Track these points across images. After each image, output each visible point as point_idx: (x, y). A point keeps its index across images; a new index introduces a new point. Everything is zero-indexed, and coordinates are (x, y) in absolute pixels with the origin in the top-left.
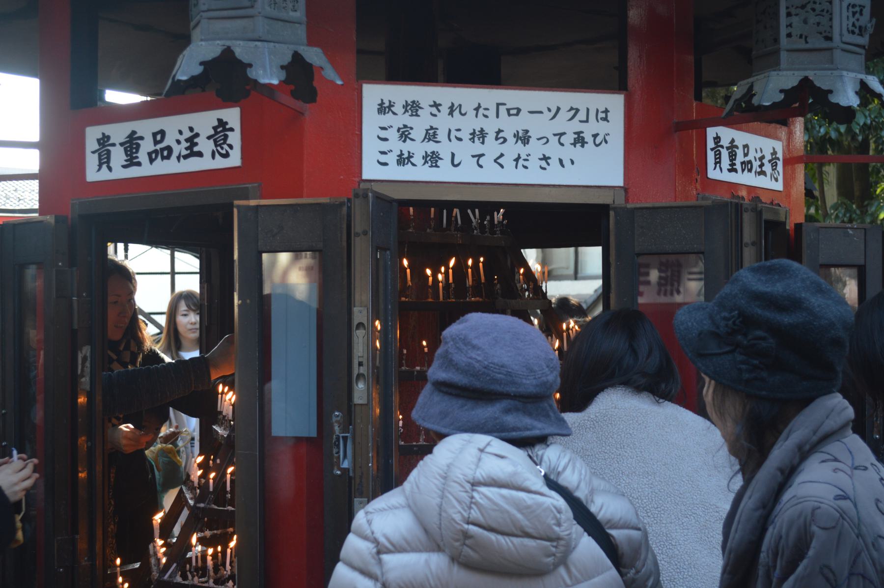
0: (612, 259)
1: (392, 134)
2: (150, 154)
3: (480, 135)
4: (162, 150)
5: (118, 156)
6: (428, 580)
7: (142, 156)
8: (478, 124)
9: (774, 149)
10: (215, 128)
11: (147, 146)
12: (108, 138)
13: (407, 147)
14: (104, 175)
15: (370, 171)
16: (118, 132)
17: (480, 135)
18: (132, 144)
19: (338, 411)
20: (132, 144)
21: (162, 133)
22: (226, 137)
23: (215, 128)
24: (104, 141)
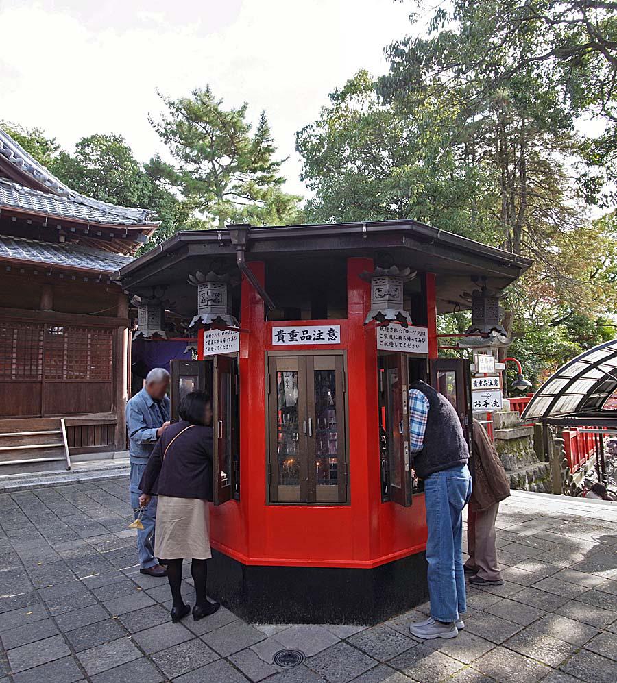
0: (448, 369)
1: (383, 336)
2: (301, 338)
3: (400, 338)
4: (307, 337)
5: (478, 384)
6: (199, 445)
7: (482, 384)
8: (401, 335)
9: (245, 107)
10: (329, 331)
11: (483, 383)
12: (283, 331)
13: (386, 340)
14: (281, 343)
15: (379, 347)
16: (478, 380)
17: (400, 338)
18: (480, 382)
19: (164, 395)
20: (480, 382)
21: (307, 331)
22: (334, 334)
23: (329, 331)
24: (475, 381)
